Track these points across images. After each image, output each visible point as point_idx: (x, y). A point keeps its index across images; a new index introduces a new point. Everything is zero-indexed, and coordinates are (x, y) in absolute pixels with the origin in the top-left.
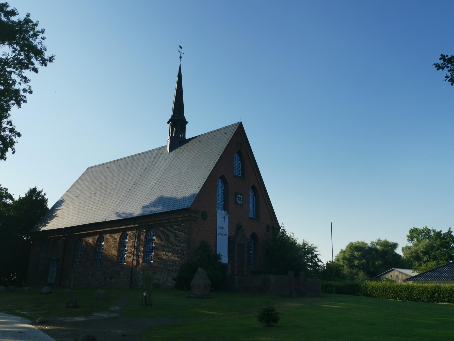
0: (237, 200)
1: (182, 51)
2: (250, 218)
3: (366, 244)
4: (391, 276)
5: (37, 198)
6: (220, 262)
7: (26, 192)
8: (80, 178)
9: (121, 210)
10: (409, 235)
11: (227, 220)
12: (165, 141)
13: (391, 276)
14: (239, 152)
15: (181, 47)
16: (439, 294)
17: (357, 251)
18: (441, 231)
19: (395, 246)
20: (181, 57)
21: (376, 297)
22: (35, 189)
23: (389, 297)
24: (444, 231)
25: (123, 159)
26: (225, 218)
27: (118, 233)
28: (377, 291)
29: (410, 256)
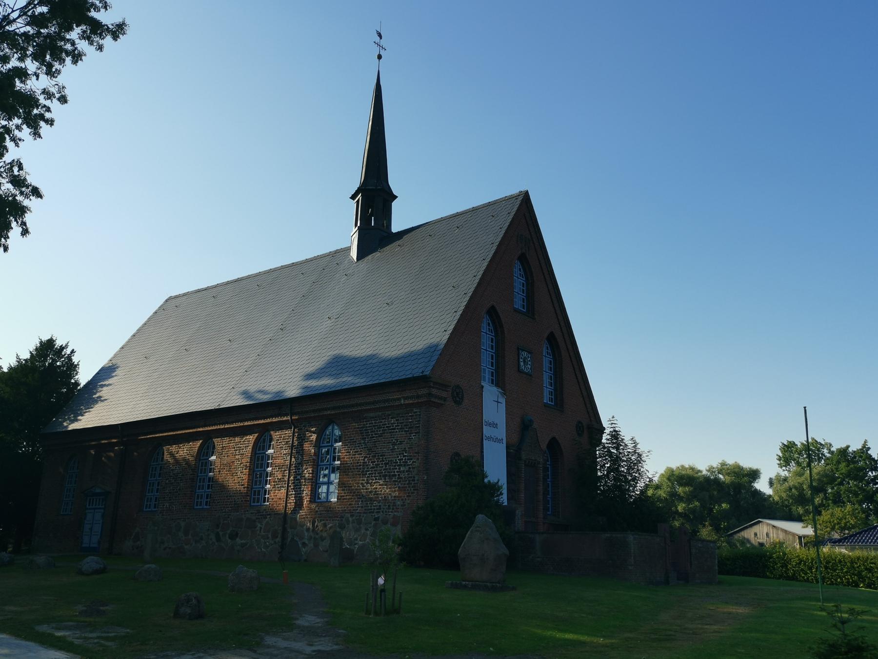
0: (522, 364)
2: (546, 405)
3: (700, 471)
4: (756, 534)
5: (54, 361)
6: (498, 501)
7: (32, 348)
8: (149, 319)
9: (252, 387)
10: (781, 455)
11: (503, 407)
12: (350, 239)
13: (756, 534)
14: (523, 259)
15: (380, 36)
17: (681, 485)
18: (848, 447)
19: (754, 475)
20: (380, 57)
21: (807, 580)
22: (51, 342)
24: (855, 446)
25: (248, 277)
26: (498, 402)
27: (251, 434)
28: (810, 569)
29: (788, 496)
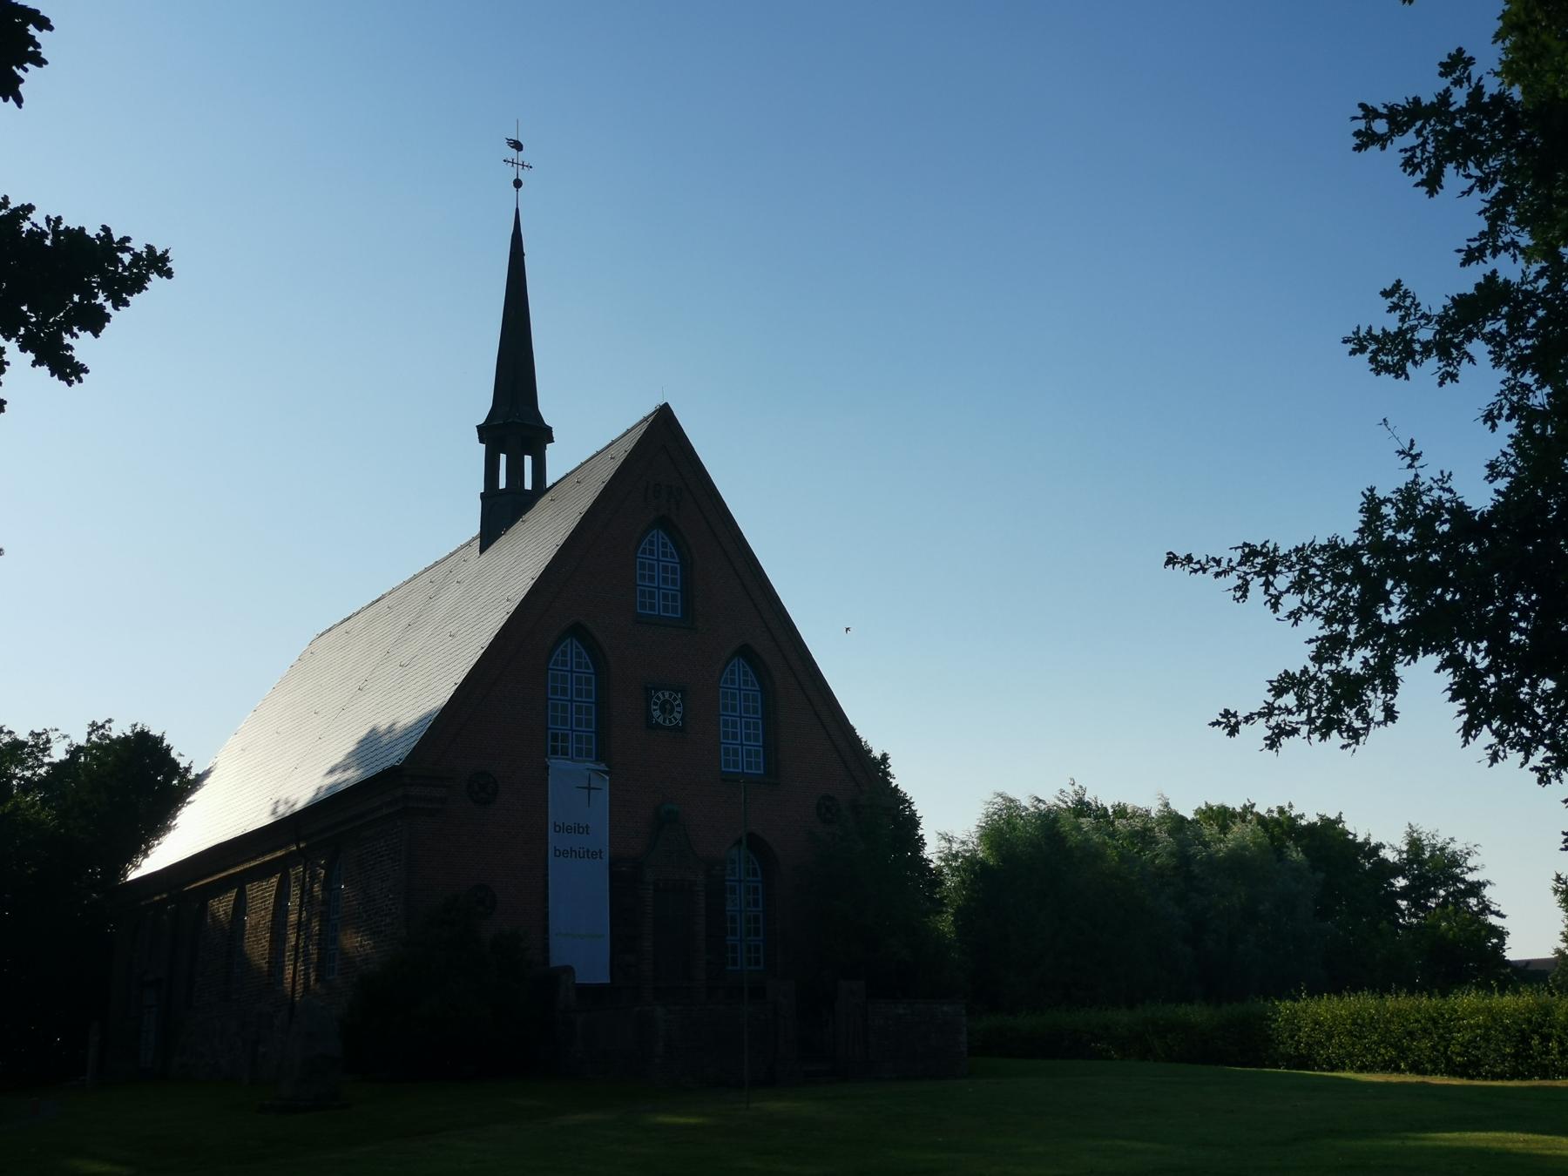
0: (656, 714)
1: (522, 156)
11: (603, 797)
15: (517, 146)
16: (1546, 1038)
20: (518, 184)
23: (1479, 1074)
26: (589, 788)
